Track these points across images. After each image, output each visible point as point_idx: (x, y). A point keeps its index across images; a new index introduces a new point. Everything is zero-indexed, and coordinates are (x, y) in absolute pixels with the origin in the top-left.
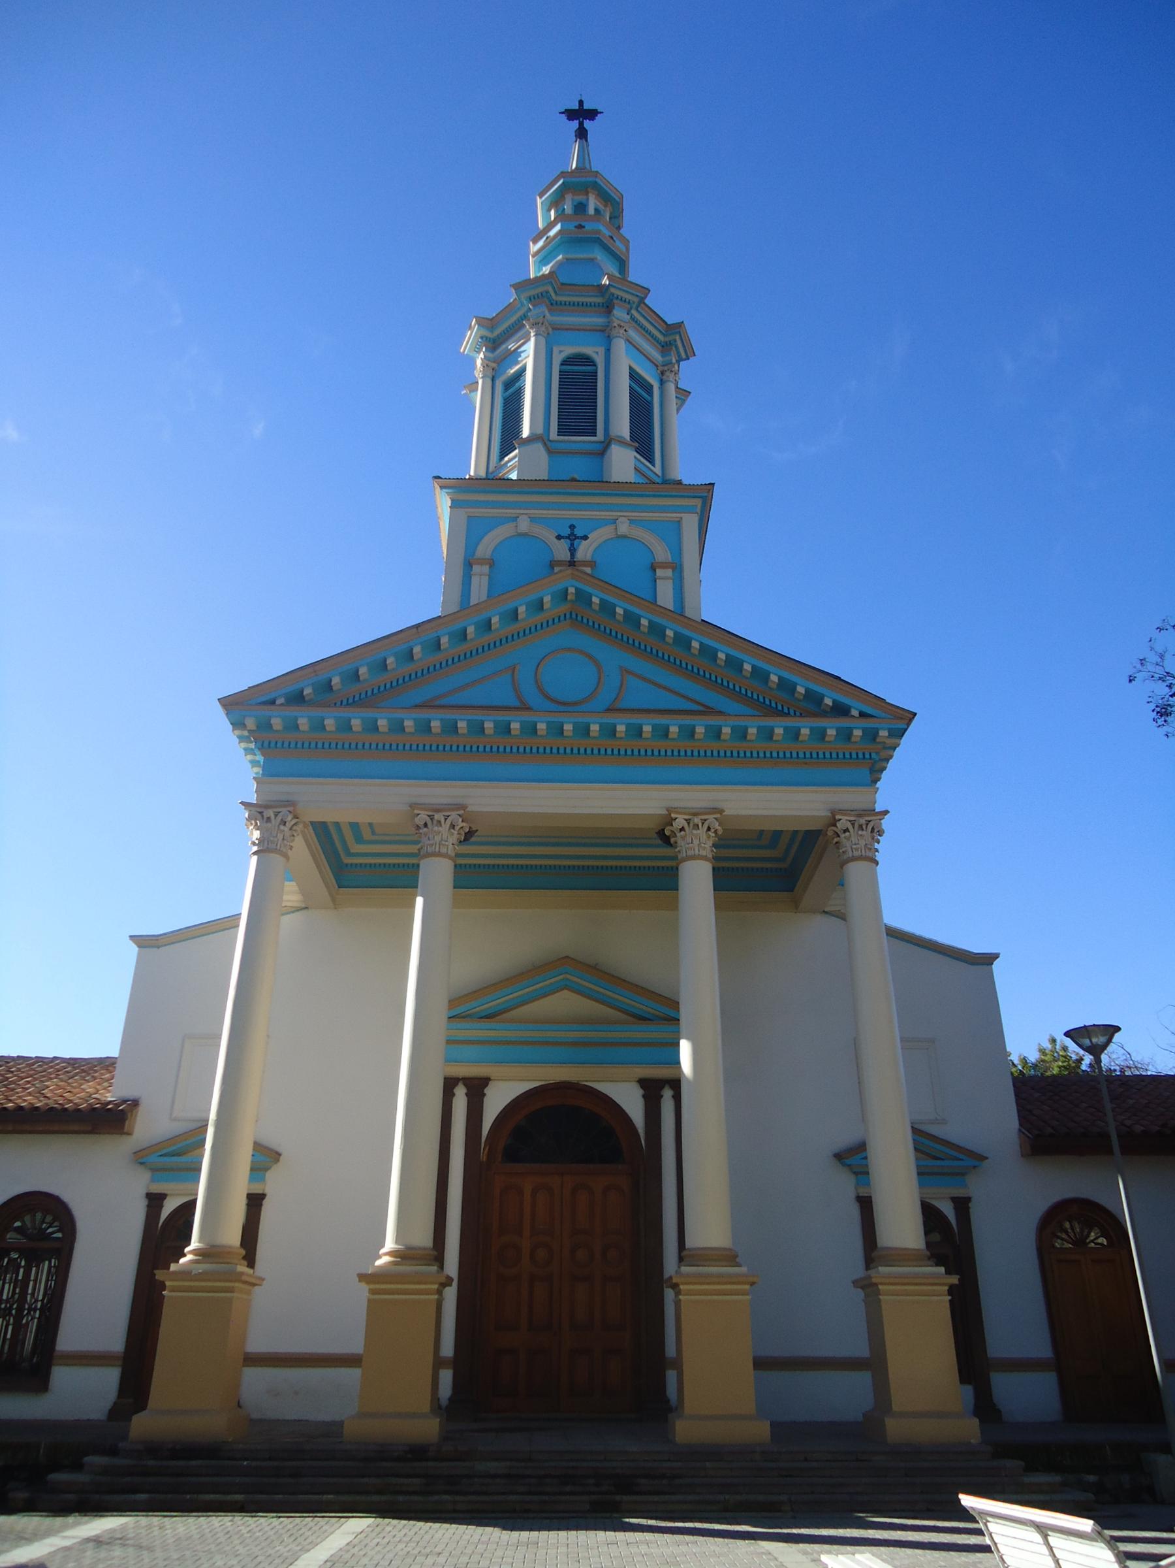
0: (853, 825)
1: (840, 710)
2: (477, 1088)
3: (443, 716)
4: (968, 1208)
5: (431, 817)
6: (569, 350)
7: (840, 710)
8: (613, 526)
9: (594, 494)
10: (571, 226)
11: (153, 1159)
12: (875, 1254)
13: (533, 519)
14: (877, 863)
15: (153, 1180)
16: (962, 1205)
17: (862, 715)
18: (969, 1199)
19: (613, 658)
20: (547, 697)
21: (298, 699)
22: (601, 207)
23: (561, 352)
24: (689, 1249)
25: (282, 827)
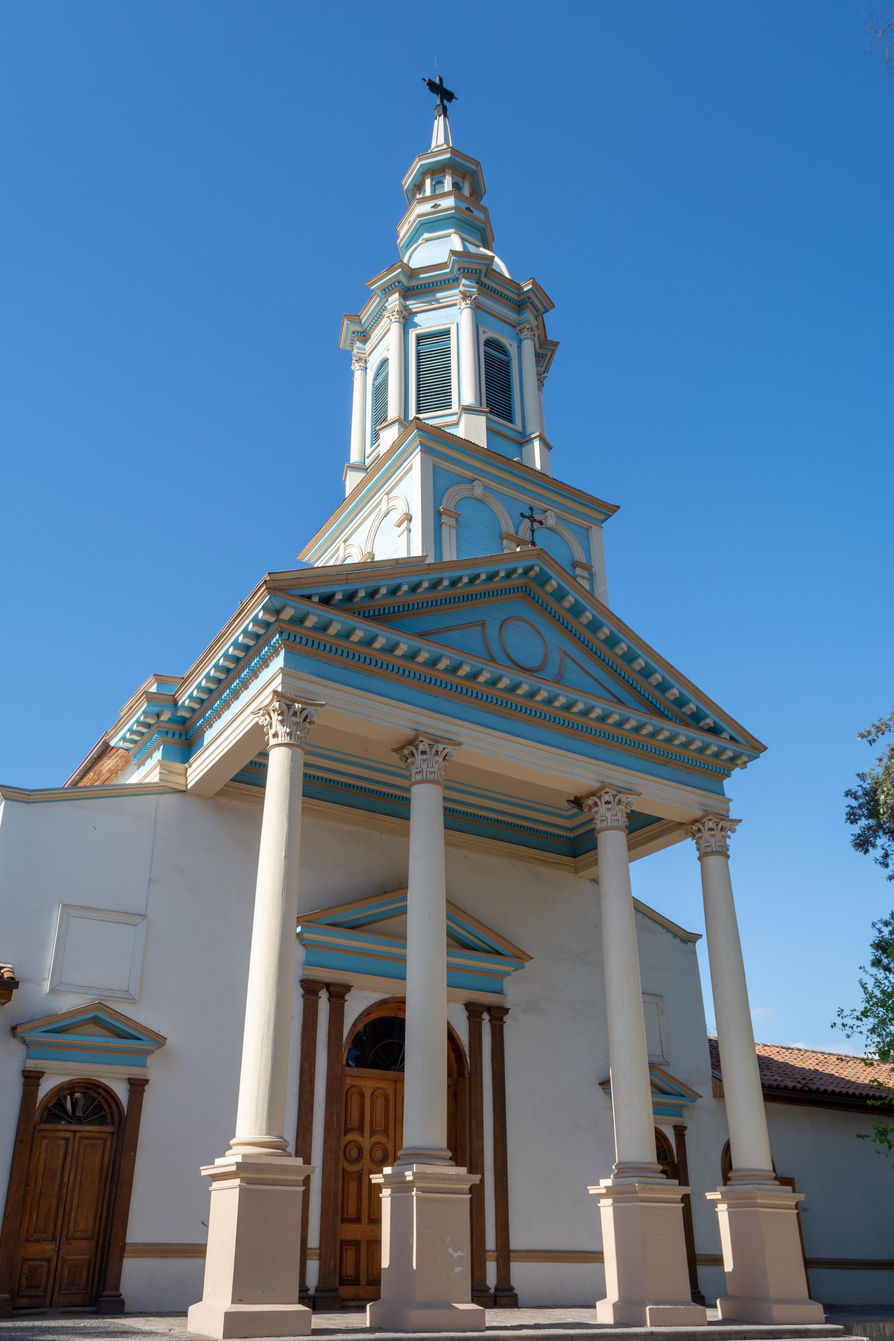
0: (289, 709)
1: (714, 731)
2: (338, 994)
3: (639, 718)
4: (684, 1135)
5: (614, 797)
6: (490, 334)
7: (714, 731)
8: (469, 486)
9: (552, 491)
10: (463, 206)
11: (35, 1036)
12: (730, 1175)
13: (485, 487)
14: (728, 857)
15: (28, 1057)
16: (680, 1131)
17: (732, 738)
18: (686, 1128)
19: (557, 640)
20: (509, 657)
21: (667, 716)
22: (459, 180)
23: (484, 332)
24: (740, 1170)
25: (437, 758)
